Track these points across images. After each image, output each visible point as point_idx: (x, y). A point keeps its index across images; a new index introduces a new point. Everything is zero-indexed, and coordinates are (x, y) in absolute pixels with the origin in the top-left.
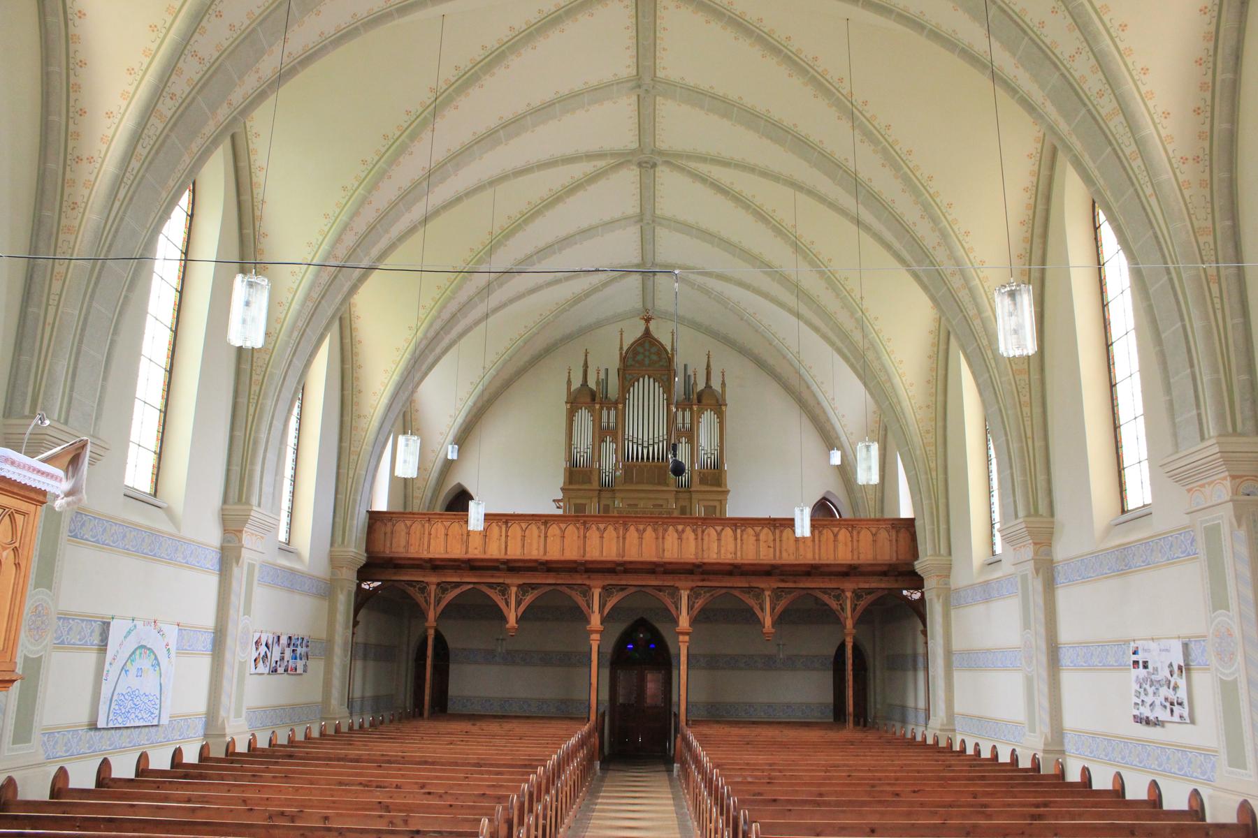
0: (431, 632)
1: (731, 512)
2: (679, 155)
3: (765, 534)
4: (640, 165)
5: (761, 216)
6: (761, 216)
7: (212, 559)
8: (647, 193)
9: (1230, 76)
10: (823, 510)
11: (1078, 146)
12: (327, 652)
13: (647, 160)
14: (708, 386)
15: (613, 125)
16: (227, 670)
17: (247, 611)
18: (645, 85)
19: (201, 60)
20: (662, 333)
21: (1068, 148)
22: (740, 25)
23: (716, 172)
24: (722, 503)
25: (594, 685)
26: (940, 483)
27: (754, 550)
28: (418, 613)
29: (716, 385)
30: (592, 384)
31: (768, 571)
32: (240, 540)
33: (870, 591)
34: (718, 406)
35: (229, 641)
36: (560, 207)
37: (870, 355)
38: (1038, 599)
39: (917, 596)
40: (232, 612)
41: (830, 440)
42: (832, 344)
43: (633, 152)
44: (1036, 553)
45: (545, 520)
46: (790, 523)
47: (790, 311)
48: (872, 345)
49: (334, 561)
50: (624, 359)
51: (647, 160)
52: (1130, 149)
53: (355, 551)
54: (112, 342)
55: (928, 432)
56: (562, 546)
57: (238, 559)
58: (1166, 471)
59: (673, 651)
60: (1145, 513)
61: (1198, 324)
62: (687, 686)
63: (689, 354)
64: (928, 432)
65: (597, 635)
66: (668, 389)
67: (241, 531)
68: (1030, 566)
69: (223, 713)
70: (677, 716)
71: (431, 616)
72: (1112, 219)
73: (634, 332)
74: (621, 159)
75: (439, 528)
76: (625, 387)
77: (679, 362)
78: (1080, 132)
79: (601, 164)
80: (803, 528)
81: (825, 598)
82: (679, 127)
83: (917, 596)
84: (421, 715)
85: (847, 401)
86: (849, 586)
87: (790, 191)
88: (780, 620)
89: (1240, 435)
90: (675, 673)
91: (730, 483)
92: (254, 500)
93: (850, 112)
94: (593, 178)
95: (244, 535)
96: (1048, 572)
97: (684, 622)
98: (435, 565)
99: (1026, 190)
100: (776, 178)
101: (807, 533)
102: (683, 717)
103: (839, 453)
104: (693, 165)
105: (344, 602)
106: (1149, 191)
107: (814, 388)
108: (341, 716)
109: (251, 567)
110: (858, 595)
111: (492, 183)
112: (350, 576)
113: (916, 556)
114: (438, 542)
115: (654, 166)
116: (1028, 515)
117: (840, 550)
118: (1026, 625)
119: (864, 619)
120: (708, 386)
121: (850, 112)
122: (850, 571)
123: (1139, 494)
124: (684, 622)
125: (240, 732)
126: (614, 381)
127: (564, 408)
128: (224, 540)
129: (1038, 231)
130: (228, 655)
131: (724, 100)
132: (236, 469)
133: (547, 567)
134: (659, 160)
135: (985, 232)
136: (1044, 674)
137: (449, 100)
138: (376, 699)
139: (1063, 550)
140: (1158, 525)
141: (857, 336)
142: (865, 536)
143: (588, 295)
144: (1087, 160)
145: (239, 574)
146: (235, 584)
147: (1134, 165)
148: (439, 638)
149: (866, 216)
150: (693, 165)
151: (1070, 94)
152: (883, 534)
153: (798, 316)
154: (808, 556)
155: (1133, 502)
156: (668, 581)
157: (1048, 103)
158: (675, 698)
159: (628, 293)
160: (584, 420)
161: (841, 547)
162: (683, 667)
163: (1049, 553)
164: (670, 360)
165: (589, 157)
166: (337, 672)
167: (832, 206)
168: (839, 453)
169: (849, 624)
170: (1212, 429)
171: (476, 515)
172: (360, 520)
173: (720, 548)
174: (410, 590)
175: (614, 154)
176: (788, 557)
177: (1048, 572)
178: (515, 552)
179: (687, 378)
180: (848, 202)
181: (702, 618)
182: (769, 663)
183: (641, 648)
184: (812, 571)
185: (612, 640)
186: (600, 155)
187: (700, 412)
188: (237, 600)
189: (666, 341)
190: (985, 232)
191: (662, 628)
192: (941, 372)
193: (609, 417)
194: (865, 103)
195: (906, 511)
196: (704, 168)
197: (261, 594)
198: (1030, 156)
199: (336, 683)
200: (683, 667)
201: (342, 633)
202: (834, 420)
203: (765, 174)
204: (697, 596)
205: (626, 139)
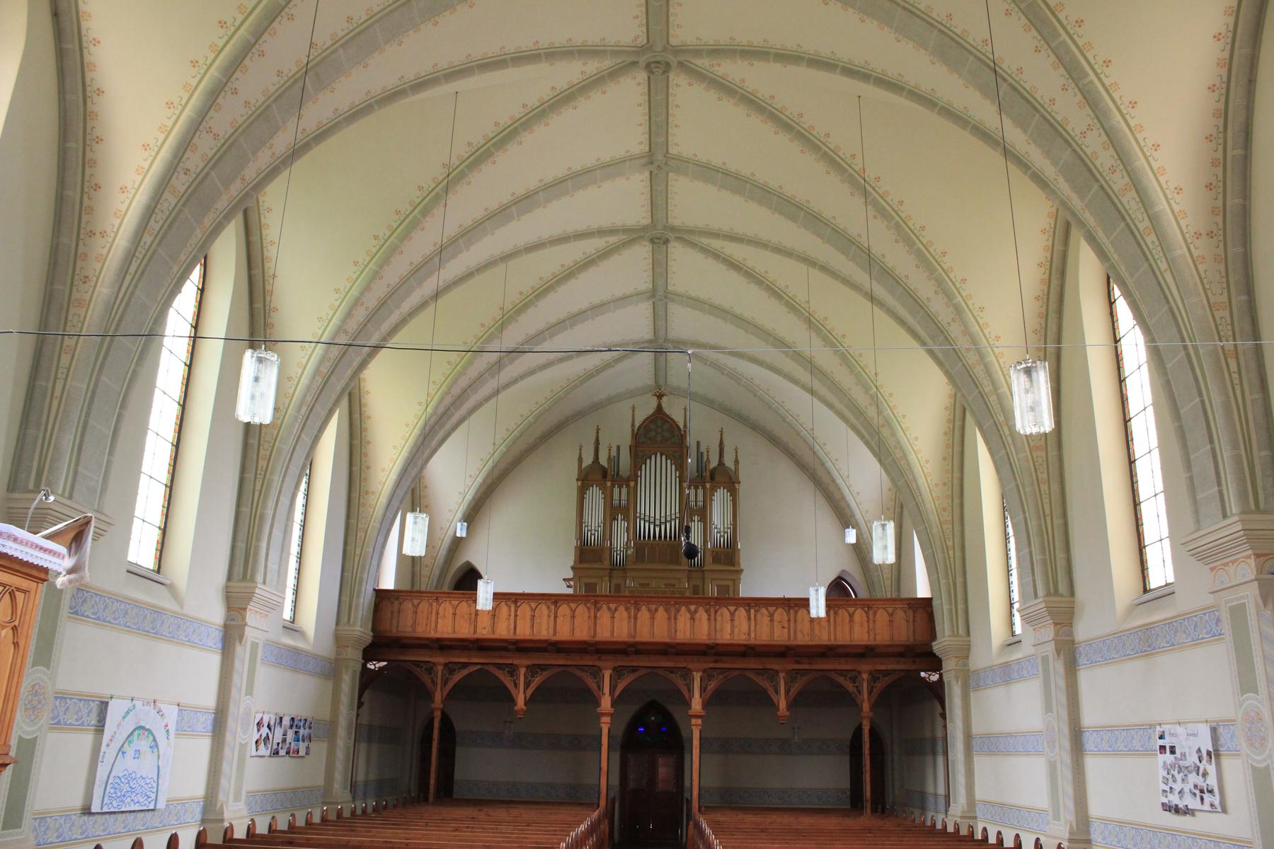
0: (438, 714)
1: (745, 591)
3: (780, 614)
4: (652, 241)
5: (774, 292)
6: (774, 292)
7: (215, 637)
8: (660, 268)
9: (1238, 201)
12: (331, 735)
13: (659, 235)
14: (721, 463)
15: (624, 201)
16: (227, 752)
17: (250, 692)
18: (658, 161)
19: (216, 136)
20: (675, 410)
21: (1082, 224)
23: (731, 249)
24: (736, 583)
26: (957, 563)
27: (767, 631)
29: (729, 462)
30: (603, 461)
32: (244, 619)
33: (887, 673)
35: (231, 722)
37: (885, 433)
38: (1059, 681)
39: (935, 677)
40: (234, 692)
41: (844, 518)
42: (846, 420)
43: (645, 228)
44: (1057, 634)
45: (554, 600)
46: (804, 603)
47: (804, 387)
48: (888, 423)
51: (659, 235)
52: (1143, 224)
55: (945, 510)
56: (572, 626)
57: (241, 637)
58: (1189, 550)
59: (684, 734)
60: (1167, 592)
63: (702, 430)
64: (945, 510)
65: (607, 716)
66: (681, 467)
67: (245, 609)
68: (1050, 648)
69: (221, 797)
70: (689, 802)
71: (438, 697)
72: (1127, 294)
73: (646, 408)
74: (632, 235)
75: (446, 607)
77: (691, 441)
78: (1093, 207)
79: (613, 239)
80: (818, 608)
81: (841, 680)
82: (693, 203)
83: (935, 677)
85: (862, 478)
86: (865, 668)
90: (687, 756)
91: (744, 562)
92: (259, 578)
93: (863, 188)
95: (248, 613)
96: (1069, 653)
97: (697, 704)
98: (443, 645)
99: (1040, 265)
100: (789, 253)
102: (695, 804)
104: (705, 241)
105: (348, 683)
106: (1163, 266)
107: (829, 464)
108: (343, 800)
110: (874, 677)
111: (506, 258)
113: (933, 637)
114: (446, 622)
115: (667, 242)
116: (1048, 594)
117: (857, 631)
118: (1048, 708)
119: (881, 702)
120: (721, 463)
121: (863, 188)
122: (866, 652)
123: (1161, 572)
124: (697, 704)
127: (574, 486)
130: (229, 736)
131: (736, 177)
132: (241, 545)
135: (1000, 309)
136: (1067, 758)
139: (1084, 630)
140: (1182, 604)
141: (871, 412)
142: (882, 616)
144: (1100, 235)
145: (242, 653)
147: (1148, 240)
148: (446, 722)
149: (879, 290)
150: (705, 241)
151: (1082, 170)
153: (812, 392)
154: (824, 637)
155: (1155, 581)
157: (1061, 180)
158: (687, 783)
159: (640, 369)
160: (595, 497)
162: (696, 752)
163: (1071, 634)
164: (682, 437)
166: (340, 754)
167: (847, 282)
169: (866, 706)
172: (365, 599)
173: (733, 629)
175: (625, 230)
176: (803, 638)
177: (1069, 653)
178: (524, 631)
179: (700, 456)
180: (862, 277)
182: (784, 747)
186: (612, 231)
187: (713, 490)
189: (678, 418)
190: (1000, 309)
193: (620, 495)
195: (923, 591)
196: (716, 244)
197: (264, 674)
198: (1043, 231)
199: (339, 766)
200: (696, 752)
202: (849, 498)
203: (778, 250)
204: (710, 677)
205: (637, 214)
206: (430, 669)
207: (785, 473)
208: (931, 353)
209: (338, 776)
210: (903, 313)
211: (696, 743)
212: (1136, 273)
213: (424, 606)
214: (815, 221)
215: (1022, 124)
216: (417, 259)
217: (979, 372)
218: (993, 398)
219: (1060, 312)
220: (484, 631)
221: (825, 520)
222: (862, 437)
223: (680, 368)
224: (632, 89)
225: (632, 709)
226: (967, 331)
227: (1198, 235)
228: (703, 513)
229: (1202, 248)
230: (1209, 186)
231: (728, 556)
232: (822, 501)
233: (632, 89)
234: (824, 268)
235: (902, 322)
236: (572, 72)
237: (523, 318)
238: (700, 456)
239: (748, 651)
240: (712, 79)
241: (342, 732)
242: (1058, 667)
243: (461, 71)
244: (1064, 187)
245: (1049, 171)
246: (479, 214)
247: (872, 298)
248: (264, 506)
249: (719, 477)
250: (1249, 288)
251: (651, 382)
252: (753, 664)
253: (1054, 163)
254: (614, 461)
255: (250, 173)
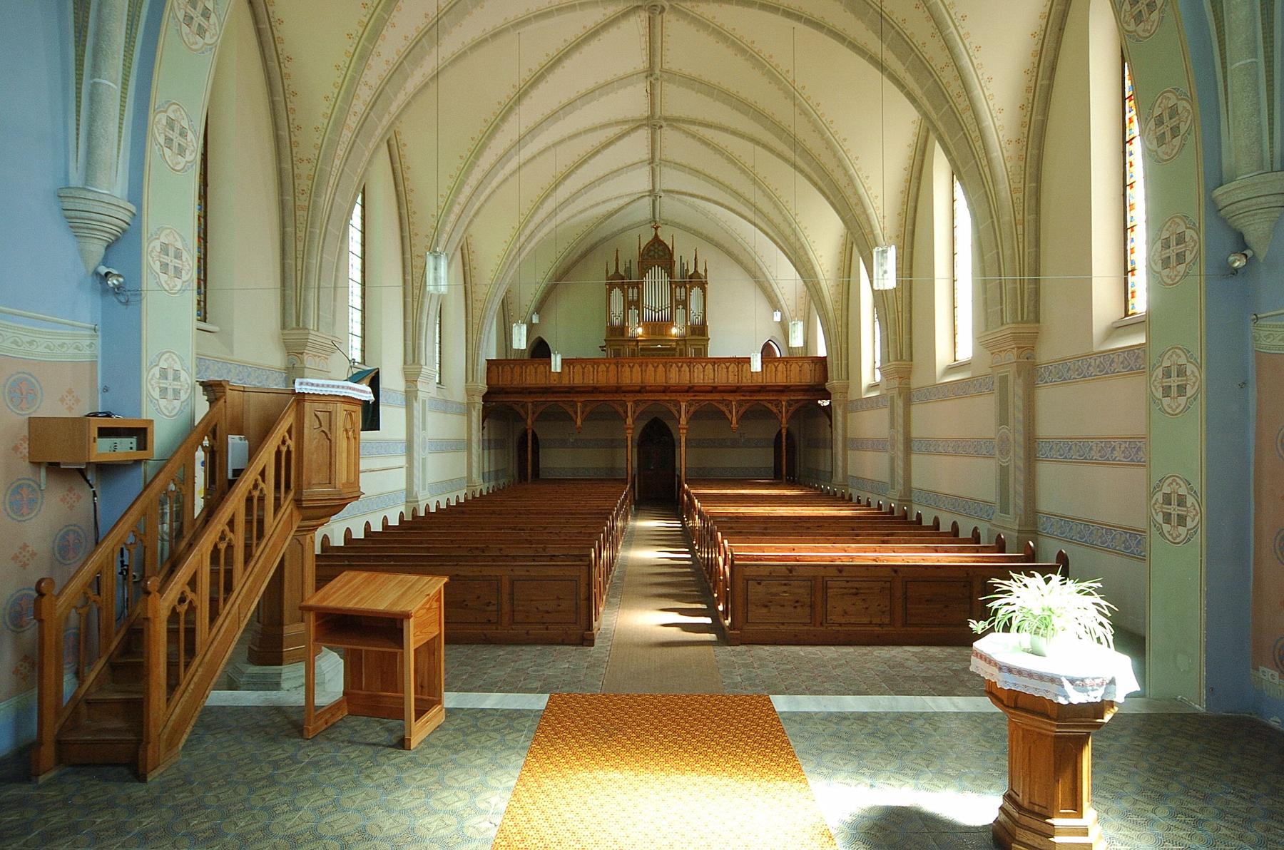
0: (530, 432)
1: (711, 354)
2: (677, 120)
3: (732, 367)
5: (732, 160)
6: (732, 160)
7: (401, 399)
9: (1046, 82)
10: (767, 350)
11: (942, 129)
12: (469, 448)
14: (696, 271)
15: (632, 102)
17: (424, 429)
18: (652, 73)
19: (371, 87)
20: (665, 236)
21: (936, 129)
22: (719, 33)
23: (703, 131)
24: (705, 347)
25: (628, 459)
26: (844, 336)
27: (726, 377)
28: (520, 419)
29: (701, 271)
30: (622, 272)
31: (736, 390)
33: (798, 401)
34: (703, 287)
36: (599, 157)
37: (801, 252)
39: (826, 403)
40: (416, 430)
41: (775, 304)
42: (776, 243)
45: (594, 362)
46: (748, 360)
47: (750, 221)
48: (802, 246)
49: (469, 392)
50: (641, 255)
51: (653, 123)
52: (975, 134)
53: (482, 386)
54: (336, 276)
56: (603, 377)
59: (675, 437)
61: (1008, 252)
62: (684, 459)
63: (683, 251)
65: (631, 429)
66: (671, 275)
68: (896, 392)
69: (416, 489)
70: (680, 477)
71: (529, 421)
72: (963, 185)
73: (647, 238)
74: (637, 125)
75: (531, 369)
76: (643, 275)
77: (677, 258)
78: (947, 118)
79: (626, 127)
80: (756, 366)
81: (769, 405)
82: (677, 101)
83: (826, 403)
84: (526, 480)
85: (786, 279)
86: (784, 399)
87: (750, 145)
88: (743, 418)
89: (1027, 322)
90: (677, 451)
91: (710, 333)
92: (423, 362)
94: (620, 137)
95: (305, 357)
97: (683, 421)
98: (530, 391)
100: (742, 136)
101: (759, 369)
102: (683, 478)
103: (779, 314)
105: (476, 415)
106: (984, 163)
107: (765, 269)
108: (481, 486)
109: (424, 402)
110: (789, 404)
111: (555, 145)
112: (479, 401)
113: (826, 379)
114: (532, 377)
116: (896, 360)
117: (780, 377)
119: (794, 417)
120: (696, 271)
122: (784, 390)
124: (683, 421)
125: (429, 500)
126: (635, 268)
127: (604, 289)
128: (407, 386)
129: (915, 174)
130: (415, 455)
131: (708, 85)
132: (410, 343)
133: (595, 390)
134: (664, 124)
137: (526, 93)
138: (497, 471)
141: (792, 239)
142: (795, 368)
143: (617, 211)
144: (947, 137)
145: (417, 406)
146: (415, 413)
147: (977, 144)
148: (534, 435)
149: (800, 162)
151: (938, 94)
152: (806, 366)
153: (755, 225)
154: (759, 381)
156: (674, 397)
158: (677, 465)
159: (642, 210)
160: (617, 295)
161: (779, 374)
162: (683, 449)
164: (671, 255)
165: (617, 123)
166: (475, 458)
167: (779, 155)
168: (779, 314)
169: (784, 420)
170: (1008, 317)
171: (556, 363)
172: (482, 366)
173: (702, 376)
174: (515, 407)
176: (746, 381)
178: (578, 381)
179: (682, 265)
180: (789, 153)
181: (695, 417)
182: (735, 444)
183: (657, 437)
184: (762, 389)
185: (639, 430)
186: (625, 122)
187: (691, 288)
188: (417, 422)
189: (668, 243)
191: (670, 424)
192: (847, 263)
193: (632, 293)
194: (804, 88)
195: (822, 352)
196: (694, 128)
197: (432, 417)
199: (475, 464)
200: (683, 449)
201: (476, 435)
202: (777, 291)
203: (734, 133)
204: (691, 405)
205: (642, 110)
206: (524, 406)
207: (736, 273)
208: (832, 204)
209: (475, 471)
210: (816, 178)
211: (683, 444)
212: (971, 169)
213: (517, 369)
214: (759, 116)
215: (902, 58)
216: (501, 152)
217: (862, 218)
218: (870, 237)
219: (919, 178)
220: (554, 382)
221: (762, 306)
222: (786, 254)
223: (669, 207)
224: (644, 133)
225: (644, 423)
226: (856, 193)
227: (1010, 142)
228: (685, 304)
229: (1010, 151)
230: (1022, 107)
231: (699, 331)
232: (758, 290)
233: (644, 133)
234: (765, 146)
235: (815, 184)
236: (616, 130)
237: (568, 182)
238: (682, 265)
239: (714, 389)
240: (693, 17)
241: (475, 445)
242: (899, 403)
243: (523, 22)
244: (925, 102)
245: (918, 92)
246: (539, 118)
247: (795, 166)
248: (421, 318)
249: (697, 281)
250: (1038, 178)
251: (649, 216)
252: (717, 397)
253: (922, 88)
254: (628, 270)
255: (394, 108)
